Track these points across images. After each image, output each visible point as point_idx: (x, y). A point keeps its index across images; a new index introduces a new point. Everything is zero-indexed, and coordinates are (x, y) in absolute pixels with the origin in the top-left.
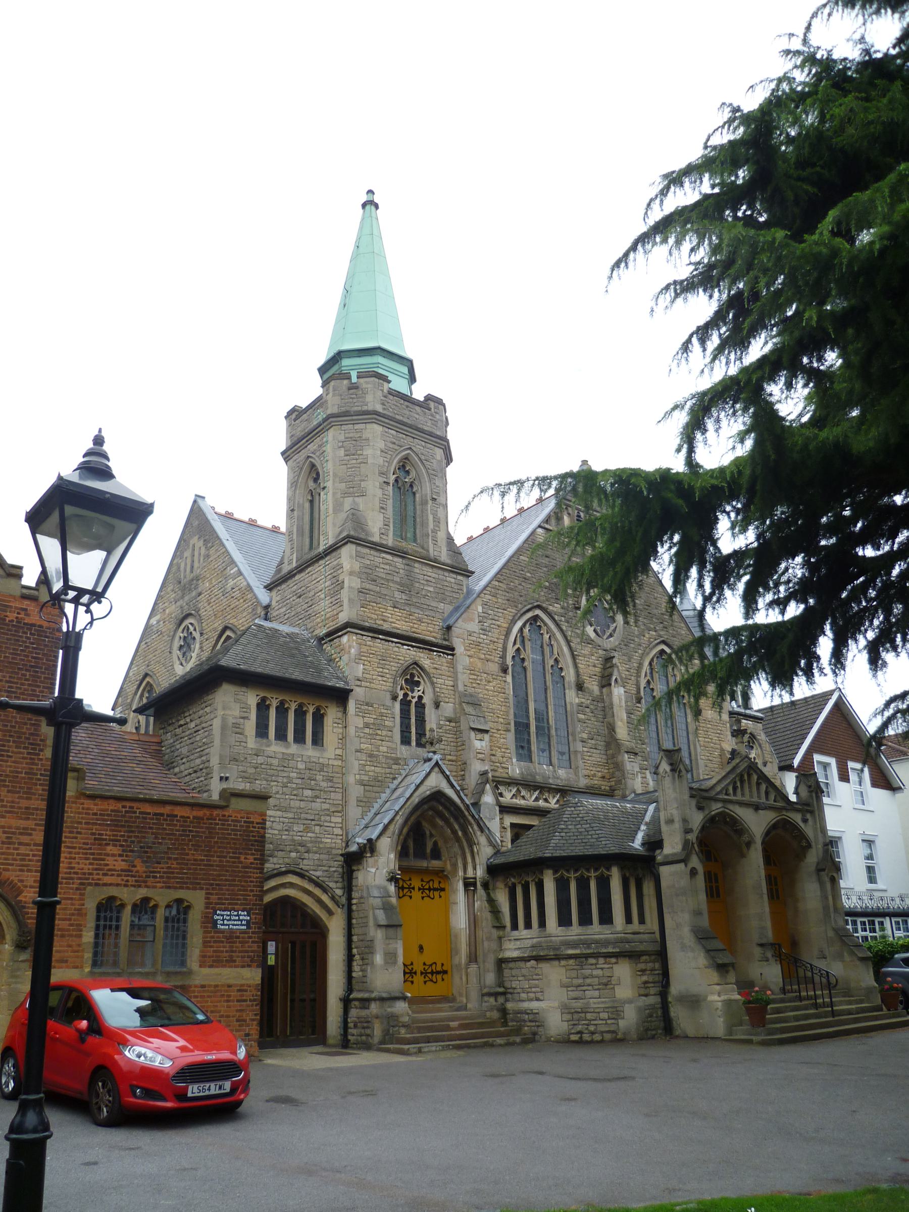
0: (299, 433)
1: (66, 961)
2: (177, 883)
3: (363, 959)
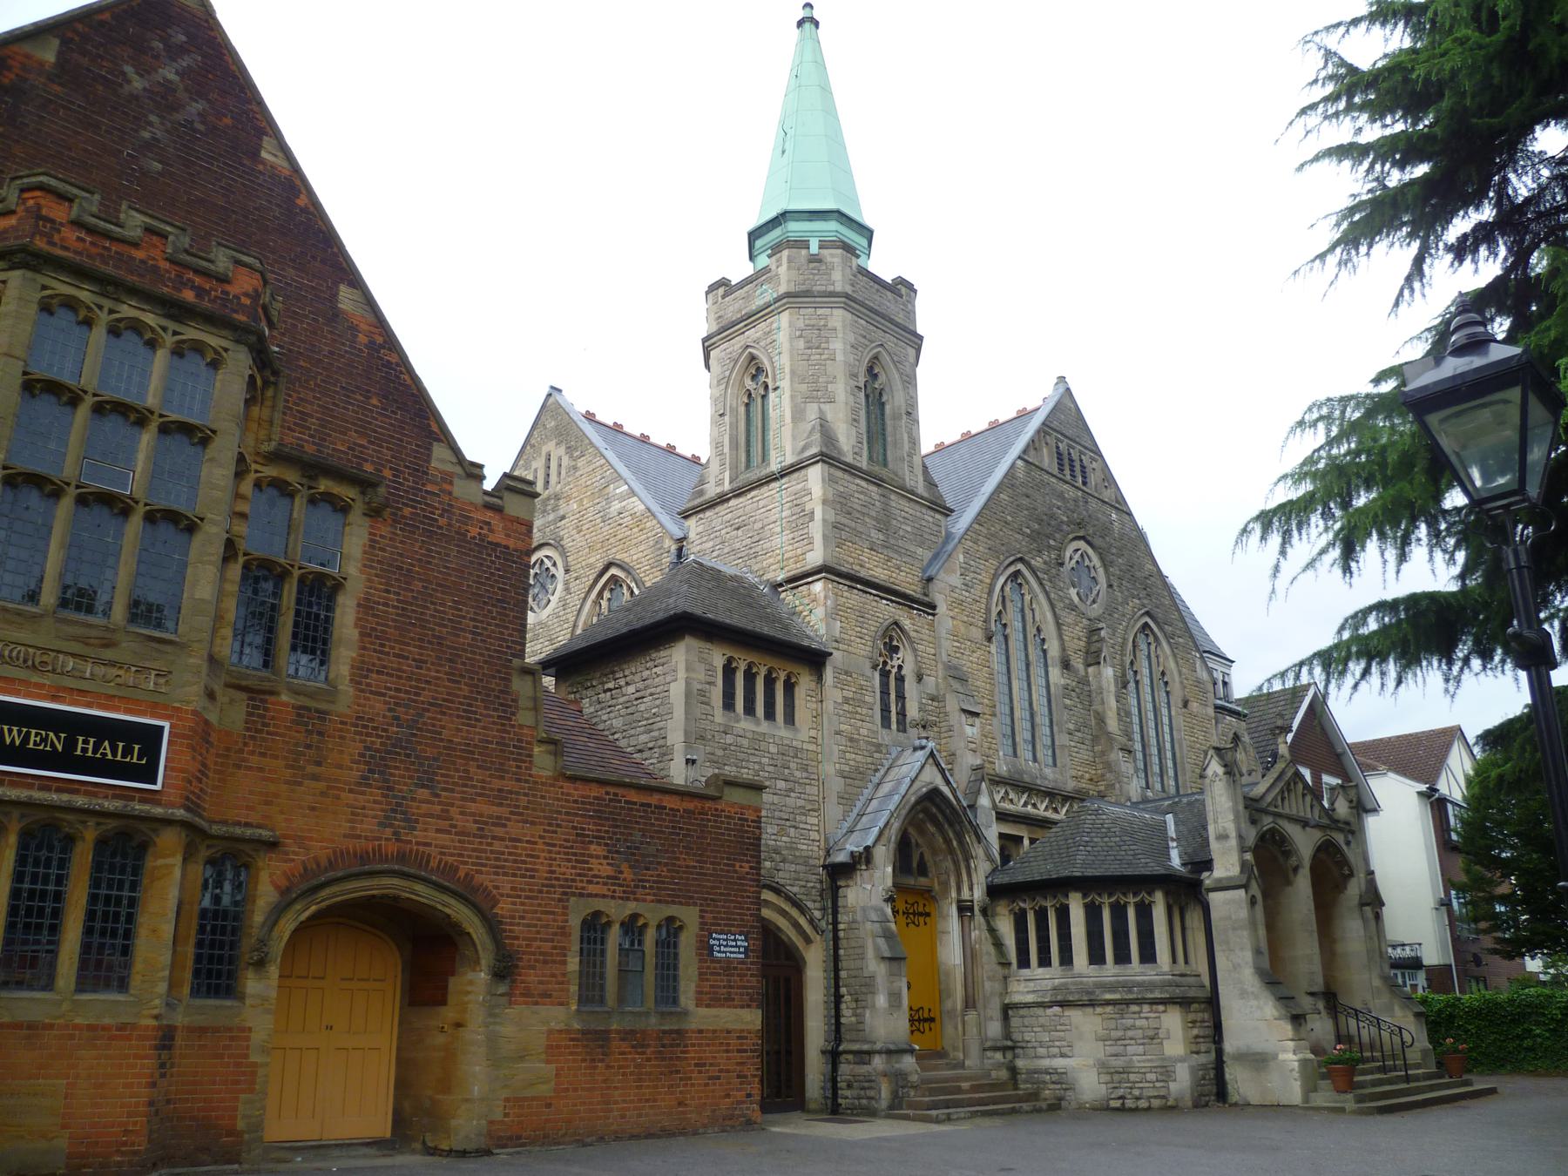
1: (550, 996)
3: (857, 1001)
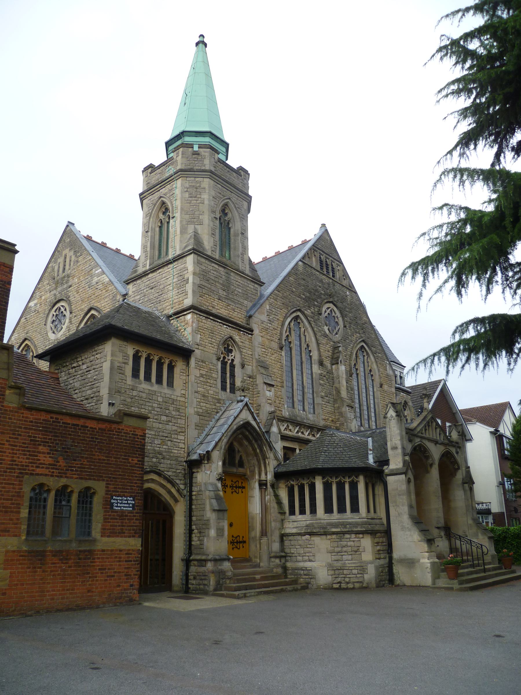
0: (154, 181)
1: (8, 531)
2: (87, 475)
3: (200, 533)
